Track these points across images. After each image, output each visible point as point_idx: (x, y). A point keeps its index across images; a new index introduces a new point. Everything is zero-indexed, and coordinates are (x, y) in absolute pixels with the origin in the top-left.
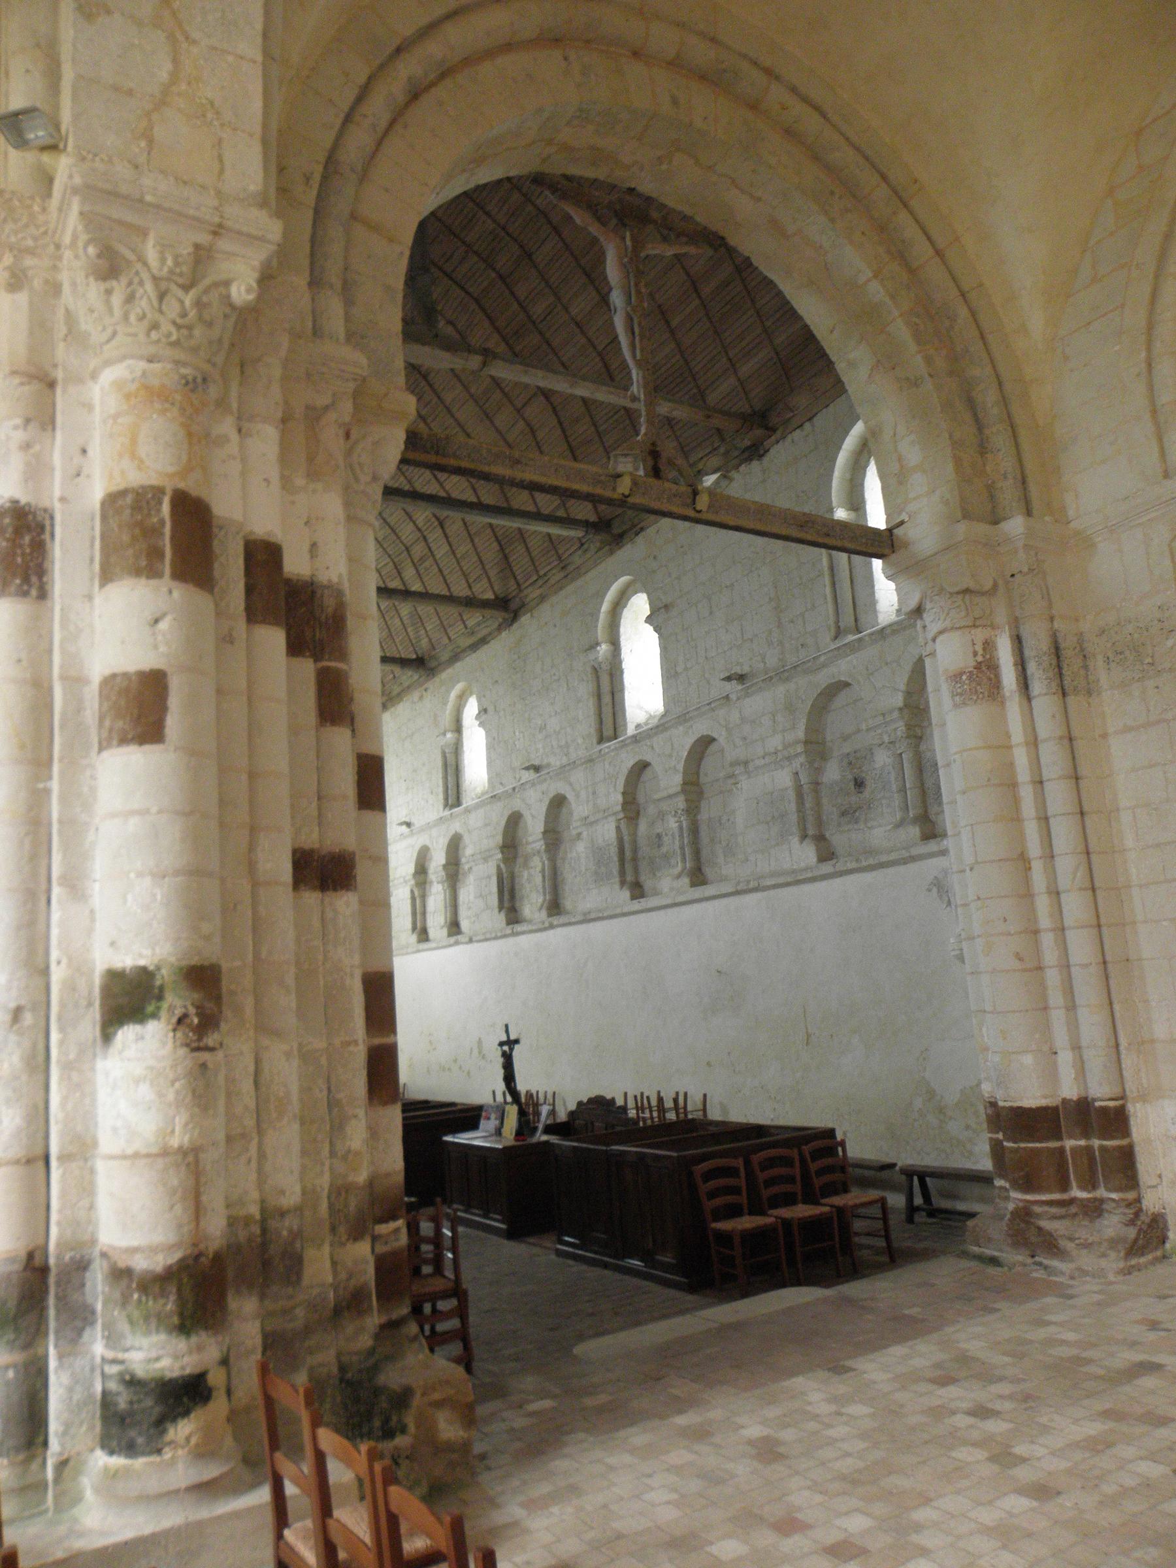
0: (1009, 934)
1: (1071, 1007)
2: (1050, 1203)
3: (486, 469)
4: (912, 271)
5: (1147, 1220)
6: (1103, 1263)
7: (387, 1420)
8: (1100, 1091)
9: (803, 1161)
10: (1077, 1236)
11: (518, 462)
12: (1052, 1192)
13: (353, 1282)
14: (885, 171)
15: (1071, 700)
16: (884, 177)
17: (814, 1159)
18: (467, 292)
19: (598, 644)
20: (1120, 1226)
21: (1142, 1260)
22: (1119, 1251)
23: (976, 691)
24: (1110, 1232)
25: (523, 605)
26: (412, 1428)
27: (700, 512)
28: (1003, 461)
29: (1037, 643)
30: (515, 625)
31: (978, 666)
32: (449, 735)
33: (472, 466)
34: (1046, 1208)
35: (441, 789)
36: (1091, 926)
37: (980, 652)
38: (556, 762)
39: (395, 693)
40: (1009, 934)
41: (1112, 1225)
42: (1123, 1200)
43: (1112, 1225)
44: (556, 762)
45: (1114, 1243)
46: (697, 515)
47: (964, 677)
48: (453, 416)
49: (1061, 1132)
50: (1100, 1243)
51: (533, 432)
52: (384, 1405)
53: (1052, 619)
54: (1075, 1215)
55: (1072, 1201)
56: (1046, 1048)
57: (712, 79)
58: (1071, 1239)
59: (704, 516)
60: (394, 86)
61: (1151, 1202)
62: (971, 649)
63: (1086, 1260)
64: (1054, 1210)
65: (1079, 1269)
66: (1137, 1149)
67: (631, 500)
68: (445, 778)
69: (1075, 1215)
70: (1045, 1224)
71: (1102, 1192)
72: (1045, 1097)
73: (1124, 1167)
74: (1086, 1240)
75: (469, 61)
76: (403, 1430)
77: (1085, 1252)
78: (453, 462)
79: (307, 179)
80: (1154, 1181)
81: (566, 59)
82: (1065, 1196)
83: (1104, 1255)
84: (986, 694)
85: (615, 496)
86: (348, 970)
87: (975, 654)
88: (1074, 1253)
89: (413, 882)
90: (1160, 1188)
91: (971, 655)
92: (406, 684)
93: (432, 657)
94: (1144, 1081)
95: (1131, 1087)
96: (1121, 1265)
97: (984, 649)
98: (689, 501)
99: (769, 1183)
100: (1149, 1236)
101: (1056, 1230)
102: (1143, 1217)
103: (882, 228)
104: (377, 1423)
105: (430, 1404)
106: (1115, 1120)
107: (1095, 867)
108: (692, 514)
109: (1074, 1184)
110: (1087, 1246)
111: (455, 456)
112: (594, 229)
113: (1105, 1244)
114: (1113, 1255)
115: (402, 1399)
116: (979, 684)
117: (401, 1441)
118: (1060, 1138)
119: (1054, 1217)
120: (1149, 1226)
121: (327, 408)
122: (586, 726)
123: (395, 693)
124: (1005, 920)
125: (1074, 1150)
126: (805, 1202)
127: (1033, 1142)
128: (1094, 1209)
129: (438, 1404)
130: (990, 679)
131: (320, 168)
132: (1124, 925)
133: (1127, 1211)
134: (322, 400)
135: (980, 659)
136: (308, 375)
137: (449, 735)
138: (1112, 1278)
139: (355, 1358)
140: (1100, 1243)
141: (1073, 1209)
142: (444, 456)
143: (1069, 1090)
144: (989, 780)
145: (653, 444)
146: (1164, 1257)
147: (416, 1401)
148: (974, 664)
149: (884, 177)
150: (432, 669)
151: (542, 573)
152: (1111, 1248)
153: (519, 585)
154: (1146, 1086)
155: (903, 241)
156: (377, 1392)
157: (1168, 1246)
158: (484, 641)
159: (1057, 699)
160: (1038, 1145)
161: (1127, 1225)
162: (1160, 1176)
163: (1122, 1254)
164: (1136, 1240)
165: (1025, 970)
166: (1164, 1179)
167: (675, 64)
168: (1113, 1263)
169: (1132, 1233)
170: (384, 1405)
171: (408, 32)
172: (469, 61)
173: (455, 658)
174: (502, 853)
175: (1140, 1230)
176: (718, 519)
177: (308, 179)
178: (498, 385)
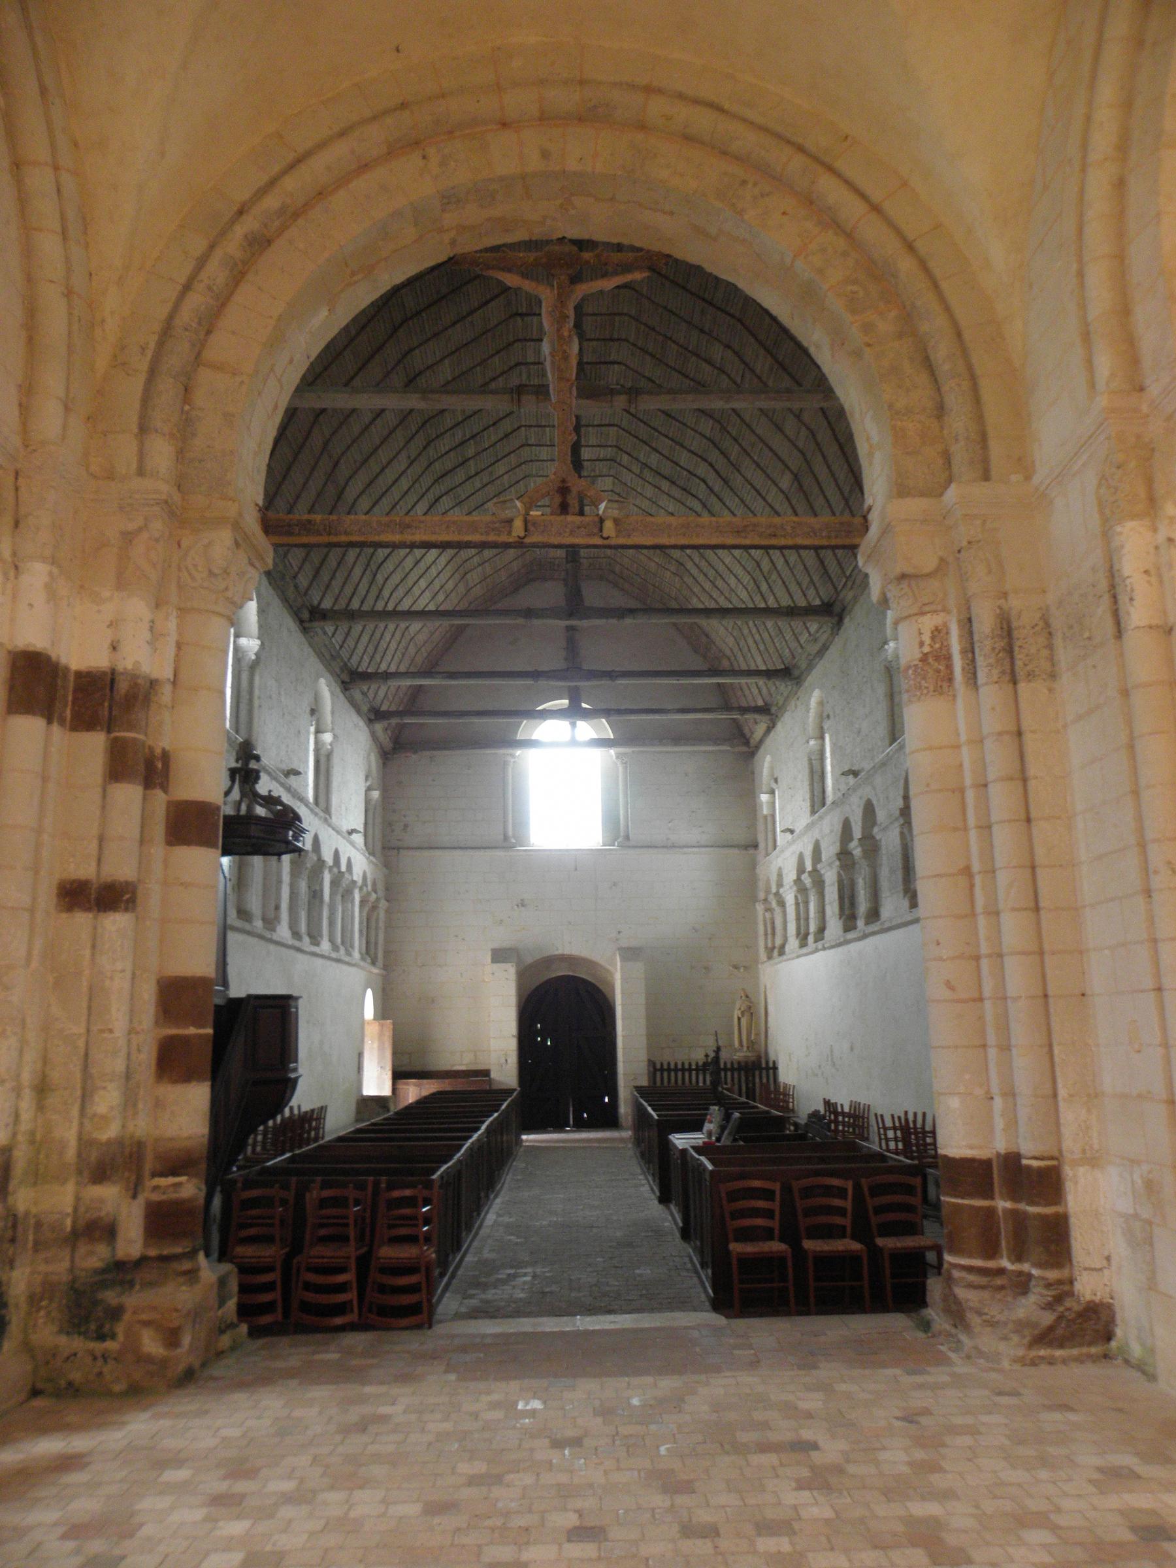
0: (941, 959)
1: (1006, 1047)
2: (970, 1269)
3: (376, 538)
4: (849, 236)
5: (1077, 1308)
6: (1002, 1347)
7: (101, 1326)
8: (1030, 1148)
9: (859, 1198)
10: (986, 1310)
11: (409, 526)
12: (970, 1256)
13: (88, 1215)
14: (800, 141)
15: (1022, 686)
16: (801, 149)
17: (873, 1194)
18: (730, 315)
19: (886, 643)
20: (1035, 1307)
21: (1059, 1353)
22: (1024, 1337)
23: (920, 687)
24: (1021, 1313)
25: (844, 609)
26: (121, 1337)
27: (608, 538)
28: (959, 422)
29: (985, 624)
30: (841, 631)
31: (924, 658)
32: (812, 742)
33: (362, 539)
34: (964, 1274)
35: (808, 796)
36: (1033, 953)
37: (928, 641)
38: (867, 765)
39: (781, 703)
40: (941, 959)
41: (1029, 1307)
42: (1043, 1278)
43: (1029, 1308)
44: (867, 765)
45: (1020, 1326)
46: (606, 542)
47: (910, 672)
48: (753, 431)
49: (992, 1190)
50: (1006, 1324)
51: (814, 435)
52: (101, 1314)
53: (1005, 595)
54: (1002, 1288)
55: (1001, 1271)
56: (979, 1092)
57: (591, 116)
58: (979, 1313)
59: (613, 542)
60: (233, 246)
61: (1087, 1287)
62: (918, 640)
63: (987, 1340)
64: (972, 1278)
65: (976, 1348)
66: (1073, 1221)
67: (527, 540)
68: (812, 784)
69: (1002, 1288)
70: (960, 1292)
71: (1026, 1267)
72: (971, 1147)
73: (1055, 1239)
74: (993, 1317)
75: (321, 194)
76: (113, 1337)
77: (989, 1329)
78: (343, 538)
79: (143, 349)
80: (1097, 1262)
81: (424, 157)
82: (991, 1264)
83: (1005, 1338)
84: (932, 688)
85: (511, 540)
86: (109, 974)
87: (922, 644)
88: (977, 1330)
89: (795, 888)
90: (1106, 1272)
91: (917, 646)
92: (785, 694)
93: (795, 666)
94: (1096, 1141)
95: (1071, 1145)
96: (1021, 1352)
97: (933, 638)
98: (596, 531)
99: (808, 1212)
100: (1086, 1328)
101: (968, 1300)
102: (1068, 1303)
103: (809, 201)
104: (93, 1327)
105: (139, 1322)
106: (1045, 1182)
107: (1040, 883)
108: (599, 541)
109: (1005, 1253)
110: (992, 1324)
111: (346, 533)
112: (528, 286)
113: (1011, 1326)
114: (1015, 1338)
115: (116, 1313)
116: (924, 678)
117: (111, 1345)
118: (992, 1198)
119: (971, 1286)
120: (1080, 1315)
121: (140, 530)
122: (882, 730)
123: (781, 703)
124: (938, 944)
125: (1005, 1210)
126: (853, 1238)
127: (956, 1196)
128: (1022, 1285)
129: (147, 1324)
130: (938, 671)
131: (155, 337)
132: (1081, 952)
133: (1045, 1292)
134: (131, 526)
135: (926, 649)
136: (121, 508)
137: (812, 742)
138: (1006, 1364)
139: (83, 1274)
140: (1006, 1324)
141: (999, 1281)
142: (336, 535)
143: (1001, 1145)
144: (928, 785)
145: (563, 481)
146: (1106, 1356)
147: (127, 1317)
148: (919, 656)
149: (801, 149)
150: (798, 678)
151: (848, 573)
152: (1016, 1331)
153: (836, 589)
154: (1096, 1147)
155: (830, 208)
156: (95, 1303)
157: (1113, 1344)
158: (825, 648)
159: (1011, 685)
160: (960, 1201)
161: (1043, 1309)
162: (1108, 1258)
163: (1026, 1341)
164: (1051, 1328)
165: (958, 1001)
166: (1113, 1262)
167: (544, 118)
168: (1010, 1349)
169: (1048, 1318)
170: (101, 1314)
171: (246, 195)
172: (321, 194)
173: (810, 666)
174: (839, 859)
175: (1061, 1317)
176: (630, 542)
177: (143, 349)
178: (670, 416)
